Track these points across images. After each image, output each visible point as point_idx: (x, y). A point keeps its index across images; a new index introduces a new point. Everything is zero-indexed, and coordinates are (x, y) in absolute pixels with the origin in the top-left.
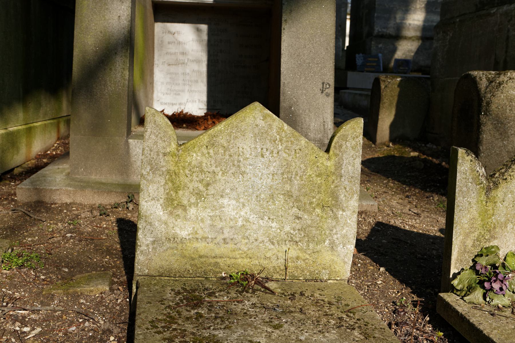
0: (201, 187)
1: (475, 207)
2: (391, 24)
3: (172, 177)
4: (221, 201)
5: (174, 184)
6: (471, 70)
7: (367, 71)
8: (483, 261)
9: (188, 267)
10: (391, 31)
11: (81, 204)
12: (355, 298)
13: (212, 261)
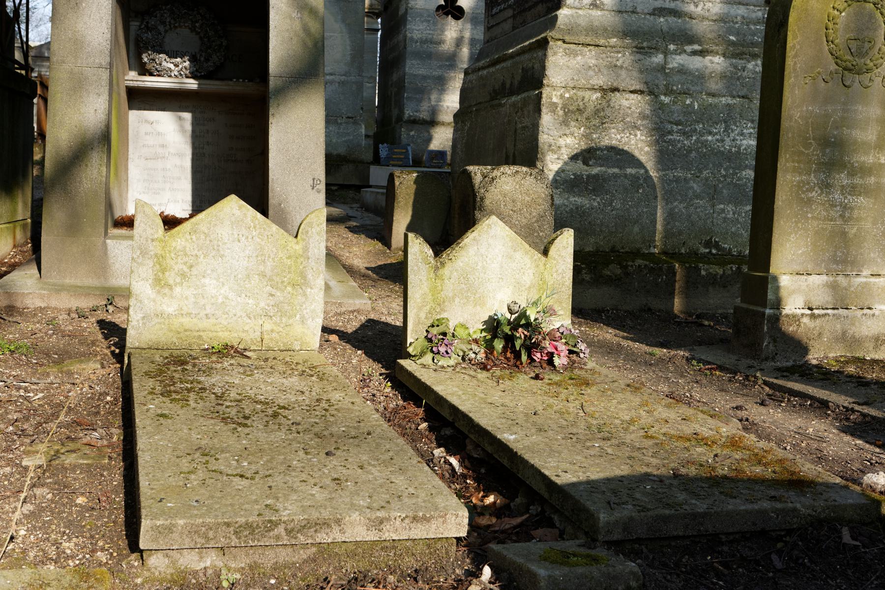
0: (185, 269)
1: (426, 284)
2: (425, 106)
3: (160, 260)
4: (203, 280)
5: (161, 267)
6: (469, 165)
7: (393, 165)
8: (434, 331)
9: (175, 340)
10: (424, 115)
11: (56, 309)
12: (319, 359)
13: (196, 334)
